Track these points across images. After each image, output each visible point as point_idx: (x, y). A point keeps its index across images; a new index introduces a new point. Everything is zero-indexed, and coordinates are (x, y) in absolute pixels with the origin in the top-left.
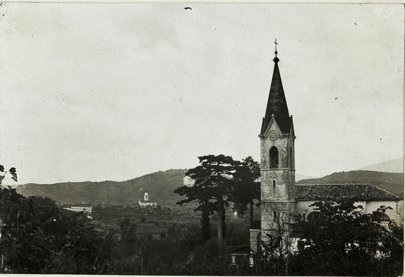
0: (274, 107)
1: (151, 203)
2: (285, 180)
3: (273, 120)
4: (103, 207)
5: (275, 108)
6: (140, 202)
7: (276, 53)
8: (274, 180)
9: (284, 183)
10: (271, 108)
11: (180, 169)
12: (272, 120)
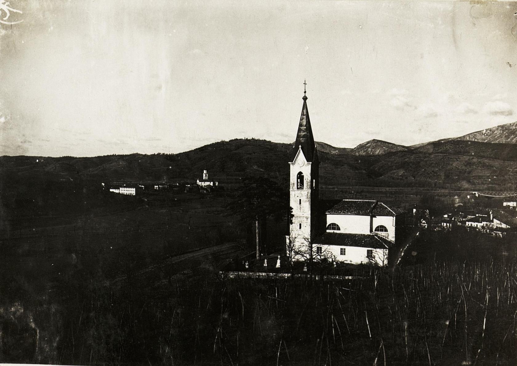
0: (302, 139)
1: (211, 182)
2: (309, 199)
3: (300, 150)
4: (156, 188)
5: (303, 140)
6: (198, 181)
7: (305, 92)
8: (300, 198)
9: (307, 202)
10: (300, 139)
11: (246, 138)
12: (299, 150)
